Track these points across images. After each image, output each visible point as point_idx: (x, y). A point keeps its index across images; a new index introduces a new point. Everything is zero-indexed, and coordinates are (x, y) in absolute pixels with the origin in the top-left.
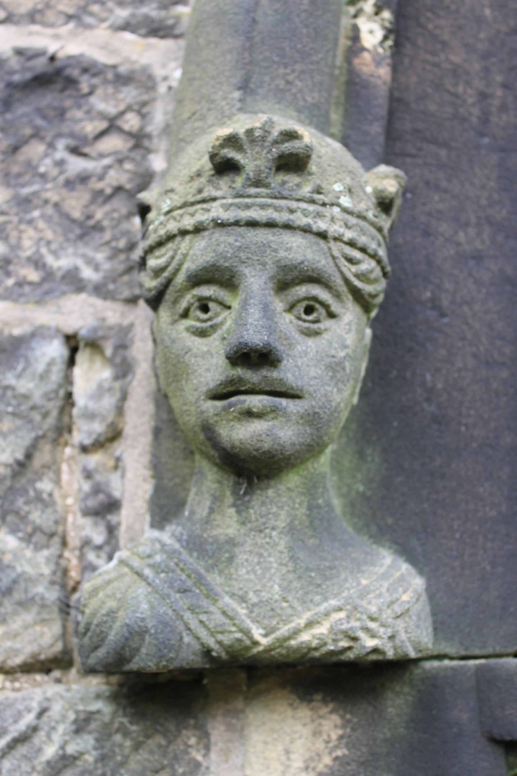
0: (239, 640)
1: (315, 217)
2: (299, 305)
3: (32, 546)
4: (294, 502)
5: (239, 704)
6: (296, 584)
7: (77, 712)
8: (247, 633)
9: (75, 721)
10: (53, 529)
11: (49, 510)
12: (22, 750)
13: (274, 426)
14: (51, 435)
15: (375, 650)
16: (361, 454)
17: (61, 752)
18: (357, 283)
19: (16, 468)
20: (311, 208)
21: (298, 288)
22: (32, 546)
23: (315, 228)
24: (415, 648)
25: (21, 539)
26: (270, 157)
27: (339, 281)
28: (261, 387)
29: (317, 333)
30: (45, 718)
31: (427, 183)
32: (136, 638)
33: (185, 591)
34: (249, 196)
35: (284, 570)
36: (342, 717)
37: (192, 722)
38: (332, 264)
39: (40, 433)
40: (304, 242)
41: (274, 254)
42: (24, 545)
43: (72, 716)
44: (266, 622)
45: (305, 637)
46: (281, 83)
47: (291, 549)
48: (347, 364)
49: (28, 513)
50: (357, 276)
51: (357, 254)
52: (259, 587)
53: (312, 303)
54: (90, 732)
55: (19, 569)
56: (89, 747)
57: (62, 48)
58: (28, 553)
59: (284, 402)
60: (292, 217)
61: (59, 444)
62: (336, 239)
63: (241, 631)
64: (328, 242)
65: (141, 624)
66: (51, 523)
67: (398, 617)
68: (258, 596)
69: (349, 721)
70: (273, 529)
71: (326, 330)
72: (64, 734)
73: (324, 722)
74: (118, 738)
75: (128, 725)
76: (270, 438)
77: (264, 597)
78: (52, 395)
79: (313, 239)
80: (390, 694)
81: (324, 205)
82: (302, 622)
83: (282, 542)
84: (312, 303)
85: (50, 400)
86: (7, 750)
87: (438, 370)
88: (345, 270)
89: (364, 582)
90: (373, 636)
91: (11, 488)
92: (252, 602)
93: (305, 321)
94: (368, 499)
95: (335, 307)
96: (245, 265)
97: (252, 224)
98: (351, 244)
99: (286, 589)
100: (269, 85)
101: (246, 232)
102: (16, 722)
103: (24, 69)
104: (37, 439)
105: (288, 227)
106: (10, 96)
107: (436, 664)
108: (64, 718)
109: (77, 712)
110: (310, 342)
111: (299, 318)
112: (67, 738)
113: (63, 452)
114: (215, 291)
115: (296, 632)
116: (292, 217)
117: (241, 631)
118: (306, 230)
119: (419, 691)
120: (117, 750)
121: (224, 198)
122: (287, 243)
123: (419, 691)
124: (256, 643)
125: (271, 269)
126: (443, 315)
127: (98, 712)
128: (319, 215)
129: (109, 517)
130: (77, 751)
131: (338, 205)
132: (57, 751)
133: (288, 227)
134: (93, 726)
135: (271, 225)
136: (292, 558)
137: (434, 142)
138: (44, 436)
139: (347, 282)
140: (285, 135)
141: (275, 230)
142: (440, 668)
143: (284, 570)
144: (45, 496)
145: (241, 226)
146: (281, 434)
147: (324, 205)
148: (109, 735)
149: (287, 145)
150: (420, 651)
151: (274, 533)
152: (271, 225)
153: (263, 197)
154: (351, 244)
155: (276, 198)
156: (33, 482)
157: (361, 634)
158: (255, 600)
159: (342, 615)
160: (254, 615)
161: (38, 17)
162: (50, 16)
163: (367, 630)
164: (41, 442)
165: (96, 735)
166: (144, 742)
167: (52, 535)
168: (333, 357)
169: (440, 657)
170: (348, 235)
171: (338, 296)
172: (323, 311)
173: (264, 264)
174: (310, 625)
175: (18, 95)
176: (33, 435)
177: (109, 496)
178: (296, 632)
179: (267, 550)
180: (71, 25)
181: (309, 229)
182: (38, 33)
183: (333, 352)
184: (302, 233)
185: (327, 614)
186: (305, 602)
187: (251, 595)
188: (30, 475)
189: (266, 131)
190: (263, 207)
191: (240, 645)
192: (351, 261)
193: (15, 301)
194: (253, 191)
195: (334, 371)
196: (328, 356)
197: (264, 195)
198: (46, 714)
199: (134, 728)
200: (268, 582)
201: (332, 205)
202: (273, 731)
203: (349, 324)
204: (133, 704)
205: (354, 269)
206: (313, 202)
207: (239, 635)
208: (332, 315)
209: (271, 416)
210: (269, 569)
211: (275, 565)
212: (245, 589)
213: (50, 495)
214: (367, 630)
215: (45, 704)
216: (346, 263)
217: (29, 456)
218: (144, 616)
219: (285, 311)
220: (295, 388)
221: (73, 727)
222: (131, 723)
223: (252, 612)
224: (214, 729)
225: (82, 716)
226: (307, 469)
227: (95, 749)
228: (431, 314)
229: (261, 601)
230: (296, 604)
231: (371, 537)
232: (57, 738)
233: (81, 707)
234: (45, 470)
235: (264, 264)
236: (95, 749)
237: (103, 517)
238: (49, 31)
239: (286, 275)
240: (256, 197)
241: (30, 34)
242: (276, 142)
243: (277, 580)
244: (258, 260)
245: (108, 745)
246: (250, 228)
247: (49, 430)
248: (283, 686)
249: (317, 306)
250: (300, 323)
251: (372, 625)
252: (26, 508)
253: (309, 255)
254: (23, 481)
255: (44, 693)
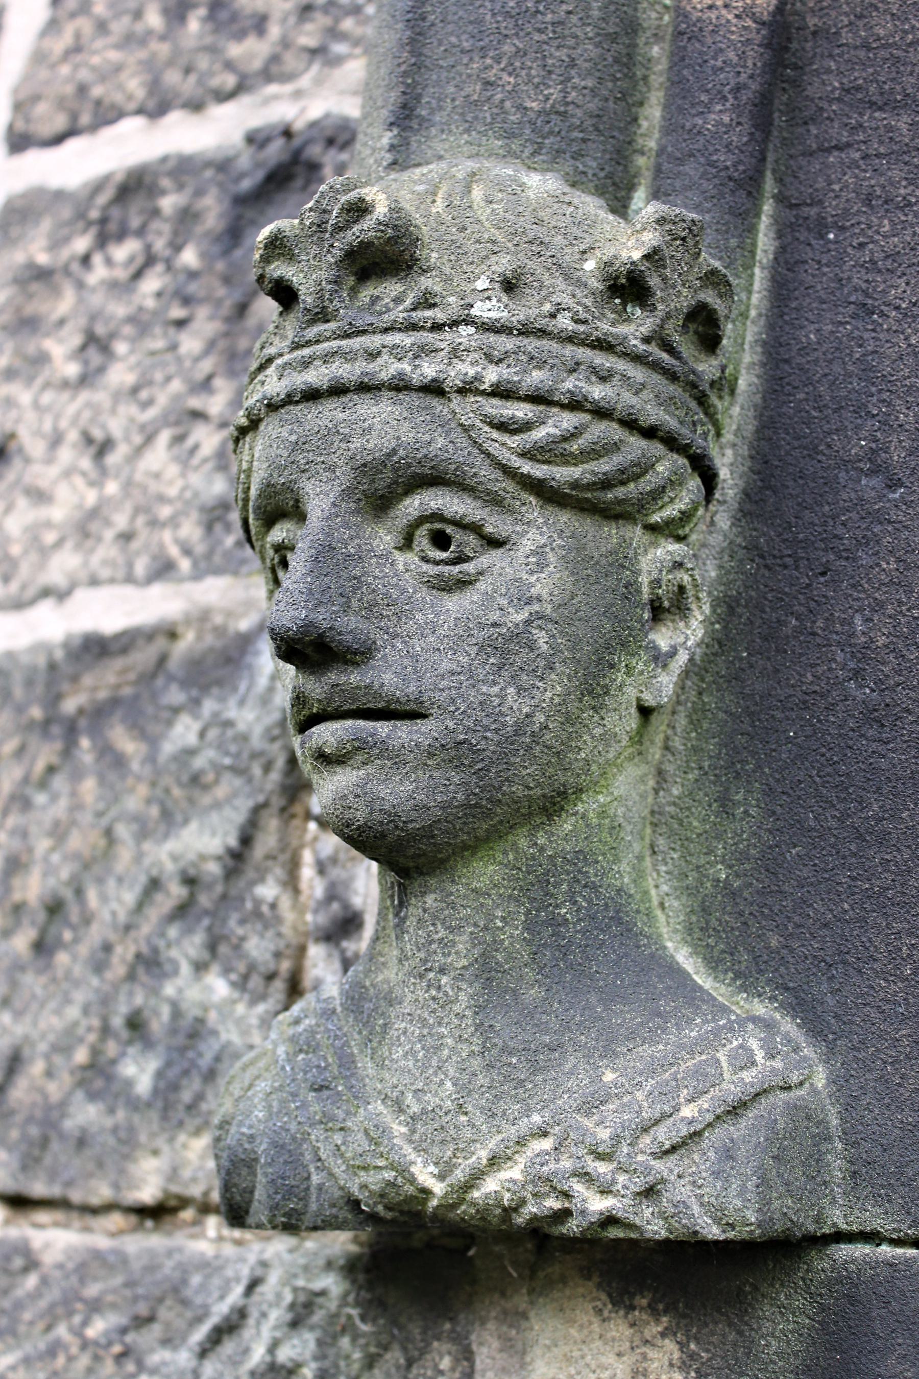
0: (391, 1184)
1: (416, 357)
2: (418, 533)
3: (247, 997)
4: (491, 918)
5: (521, 1301)
6: (482, 1080)
7: (295, 1290)
8: (403, 1170)
9: (292, 1306)
10: (272, 966)
11: (270, 934)
12: (228, 1347)
13: (367, 780)
14: (277, 802)
15: (610, 1220)
16: (724, 803)
17: (268, 1359)
18: (527, 468)
19: (230, 862)
20: (406, 340)
21: (407, 501)
22: (247, 997)
23: (416, 380)
24: (717, 1221)
25: (233, 984)
26: (332, 260)
27: (485, 473)
28: (335, 705)
29: (463, 583)
30: (255, 1298)
31: (868, 200)
32: (245, 1171)
33: (321, 1088)
34: (308, 343)
35: (465, 1050)
36: (682, 1346)
37: (448, 1326)
38: (463, 442)
39: (261, 798)
40: (397, 410)
41: (344, 445)
42: (236, 995)
43: (288, 1297)
44: (436, 1150)
45: (491, 1185)
46: (474, 89)
47: (479, 1009)
48: (541, 638)
49: (243, 939)
50: (525, 454)
51: (521, 411)
52: (420, 1085)
53: (438, 526)
54: (312, 1328)
55: (224, 1037)
56: (308, 1354)
57: (303, 111)
58: (240, 1009)
59: (383, 728)
60: (371, 367)
61: (293, 816)
62: (462, 391)
63: (392, 1167)
64: (450, 400)
65: (247, 1146)
66: (268, 956)
67: (667, 1152)
68: (419, 1100)
69: (693, 1356)
70: (442, 971)
71: (481, 573)
72: (275, 1328)
73: (652, 1353)
74: (345, 1342)
75: (358, 1322)
76: (361, 801)
77: (428, 1103)
78: (276, 732)
79: (415, 400)
80: (767, 1310)
81: (437, 327)
82: (483, 1154)
83: (462, 996)
84: (438, 526)
85: (273, 739)
86: (208, 1346)
87: (880, 605)
88: (494, 448)
89: (609, 1076)
90: (605, 1191)
91: (224, 897)
92: (411, 1112)
93: (437, 563)
94: (734, 895)
95: (494, 524)
96: (307, 475)
97: (312, 395)
98: (502, 392)
99: (464, 1089)
100: (453, 100)
101: (305, 412)
102: (222, 1298)
103: (258, 165)
104: (257, 810)
105: (365, 388)
106: (239, 218)
107: (861, 1250)
108: (279, 1296)
109: (295, 1290)
110: (454, 604)
111: (425, 559)
112: (278, 1334)
113: (305, 830)
114: (288, 531)
115: (476, 1177)
116: (371, 367)
117: (392, 1167)
118: (400, 386)
119: (823, 1308)
120: (342, 1364)
121: (281, 355)
122: (364, 421)
123: (823, 1308)
124: (426, 1192)
125: (344, 476)
126: (893, 484)
127: (323, 1293)
128: (423, 351)
129: (345, 944)
130: (292, 1360)
131: (468, 321)
132: (263, 1356)
133: (365, 388)
134: (317, 1317)
135: (337, 390)
136: (478, 1027)
137: (886, 104)
138: (265, 805)
139: (508, 472)
140: (349, 211)
141: (344, 399)
142: (866, 1262)
143: (465, 1050)
144: (265, 909)
145: (297, 403)
146: (383, 791)
147: (437, 327)
148: (335, 1337)
149: (356, 228)
150: (732, 1226)
151: (444, 980)
152: (337, 390)
153: (328, 339)
154: (502, 392)
155: (348, 336)
156: (253, 883)
157: (578, 1187)
158: (415, 1109)
159: (547, 1144)
160: (416, 1137)
161: (274, 69)
162: (291, 61)
163: (586, 1177)
164: (265, 813)
165: (318, 1333)
166: (380, 1355)
167: (270, 977)
168: (495, 625)
169: (872, 1237)
170: (491, 375)
171: (495, 501)
172: (472, 539)
173: (332, 469)
174: (495, 1162)
175: (249, 213)
176: (250, 803)
177: (346, 906)
178: (476, 1177)
179: (434, 1011)
180: (315, 68)
181: (402, 384)
182: (276, 97)
183: (495, 616)
184: (392, 394)
185: (521, 1142)
186: (493, 1115)
187: (409, 1098)
188: (250, 874)
189: (324, 211)
190: (327, 358)
191: (398, 1194)
192: (502, 426)
193: (236, 573)
194: (312, 332)
195: (504, 653)
196: (482, 626)
197: (328, 334)
198: (260, 1289)
199: (365, 1328)
200: (435, 1074)
201: (454, 324)
202: (568, 1359)
203: (539, 552)
204: (370, 1286)
205: (514, 441)
206: (413, 327)
207: (389, 1175)
208: (495, 543)
209: (359, 758)
210: (438, 1048)
211: (450, 1041)
212: (400, 1088)
213: (273, 906)
214: (586, 1177)
215: (259, 1272)
216: (495, 434)
217: (246, 840)
218: (253, 1131)
219: (399, 549)
220: (404, 700)
221: (289, 1317)
222: (363, 1318)
223: (413, 1131)
224: (481, 1344)
225: (302, 1298)
226: (515, 846)
227: (316, 1358)
228: (870, 485)
229: (424, 1112)
230: (479, 1120)
231: (738, 975)
232: (267, 1333)
233: (301, 1283)
234: (270, 863)
235: (332, 469)
236: (316, 1358)
237: (337, 944)
238: (288, 88)
239: (373, 481)
240: (318, 342)
241: (267, 101)
242: (338, 229)
243: (451, 1072)
244: (323, 462)
245: (331, 1352)
246: (310, 404)
247: (272, 792)
248: (586, 1273)
249: (449, 530)
250: (425, 567)
251: (602, 1168)
252: (240, 931)
253: (408, 434)
254: (242, 883)
255: (262, 1252)
